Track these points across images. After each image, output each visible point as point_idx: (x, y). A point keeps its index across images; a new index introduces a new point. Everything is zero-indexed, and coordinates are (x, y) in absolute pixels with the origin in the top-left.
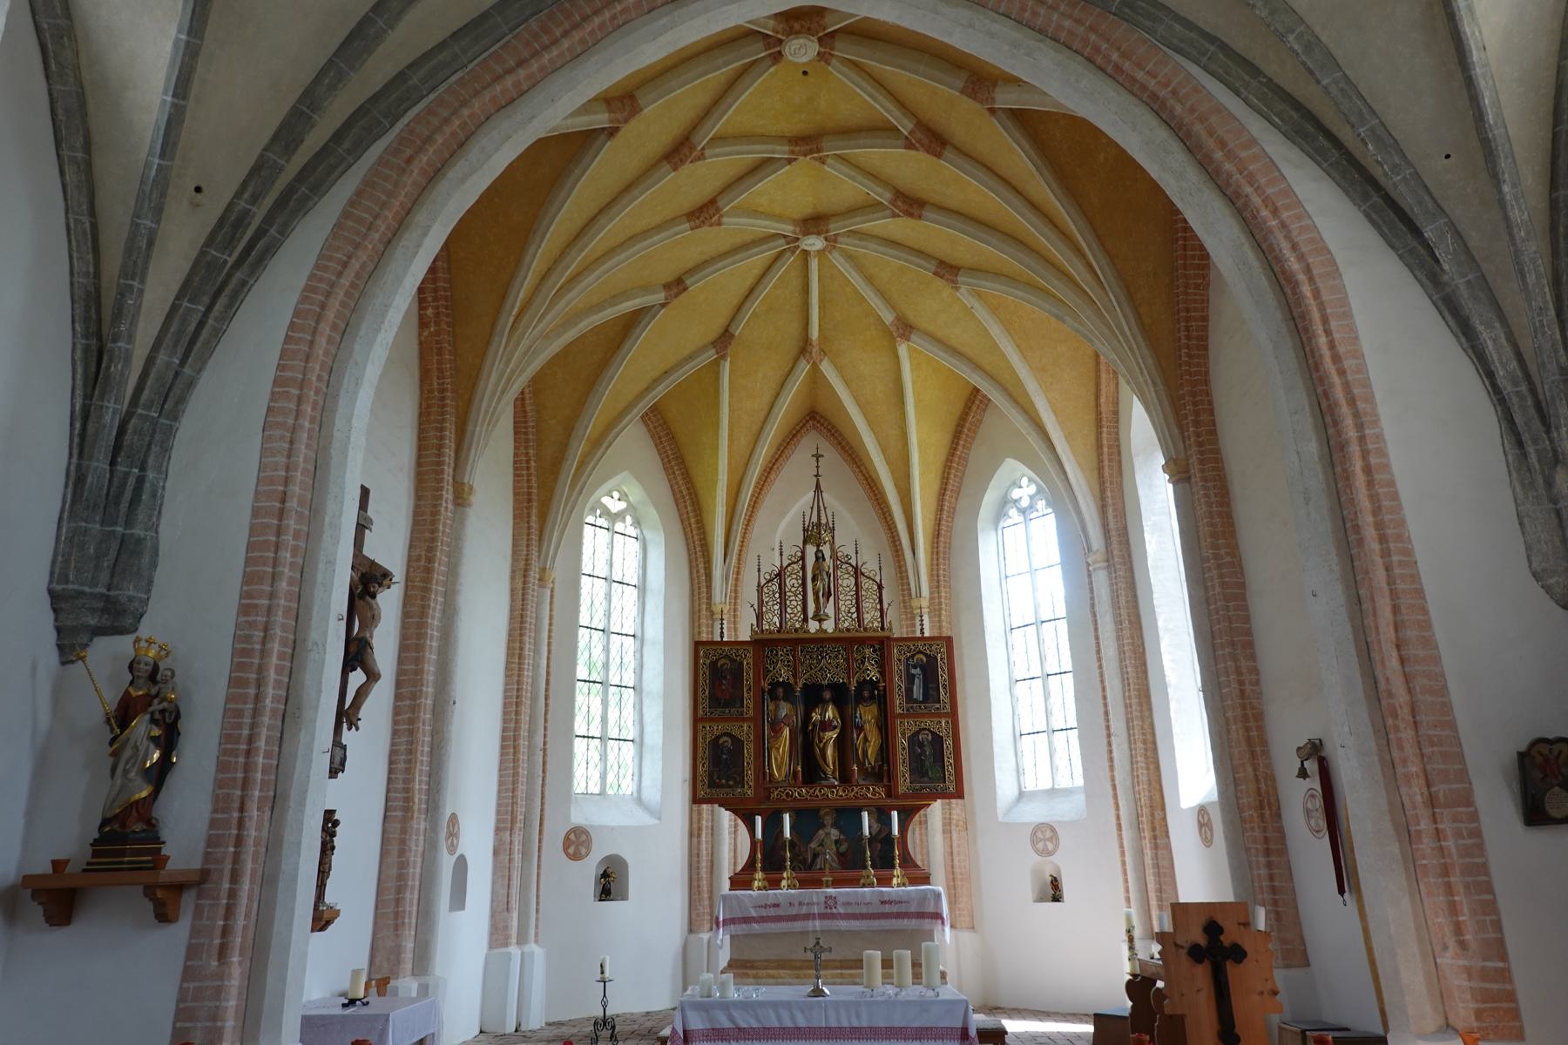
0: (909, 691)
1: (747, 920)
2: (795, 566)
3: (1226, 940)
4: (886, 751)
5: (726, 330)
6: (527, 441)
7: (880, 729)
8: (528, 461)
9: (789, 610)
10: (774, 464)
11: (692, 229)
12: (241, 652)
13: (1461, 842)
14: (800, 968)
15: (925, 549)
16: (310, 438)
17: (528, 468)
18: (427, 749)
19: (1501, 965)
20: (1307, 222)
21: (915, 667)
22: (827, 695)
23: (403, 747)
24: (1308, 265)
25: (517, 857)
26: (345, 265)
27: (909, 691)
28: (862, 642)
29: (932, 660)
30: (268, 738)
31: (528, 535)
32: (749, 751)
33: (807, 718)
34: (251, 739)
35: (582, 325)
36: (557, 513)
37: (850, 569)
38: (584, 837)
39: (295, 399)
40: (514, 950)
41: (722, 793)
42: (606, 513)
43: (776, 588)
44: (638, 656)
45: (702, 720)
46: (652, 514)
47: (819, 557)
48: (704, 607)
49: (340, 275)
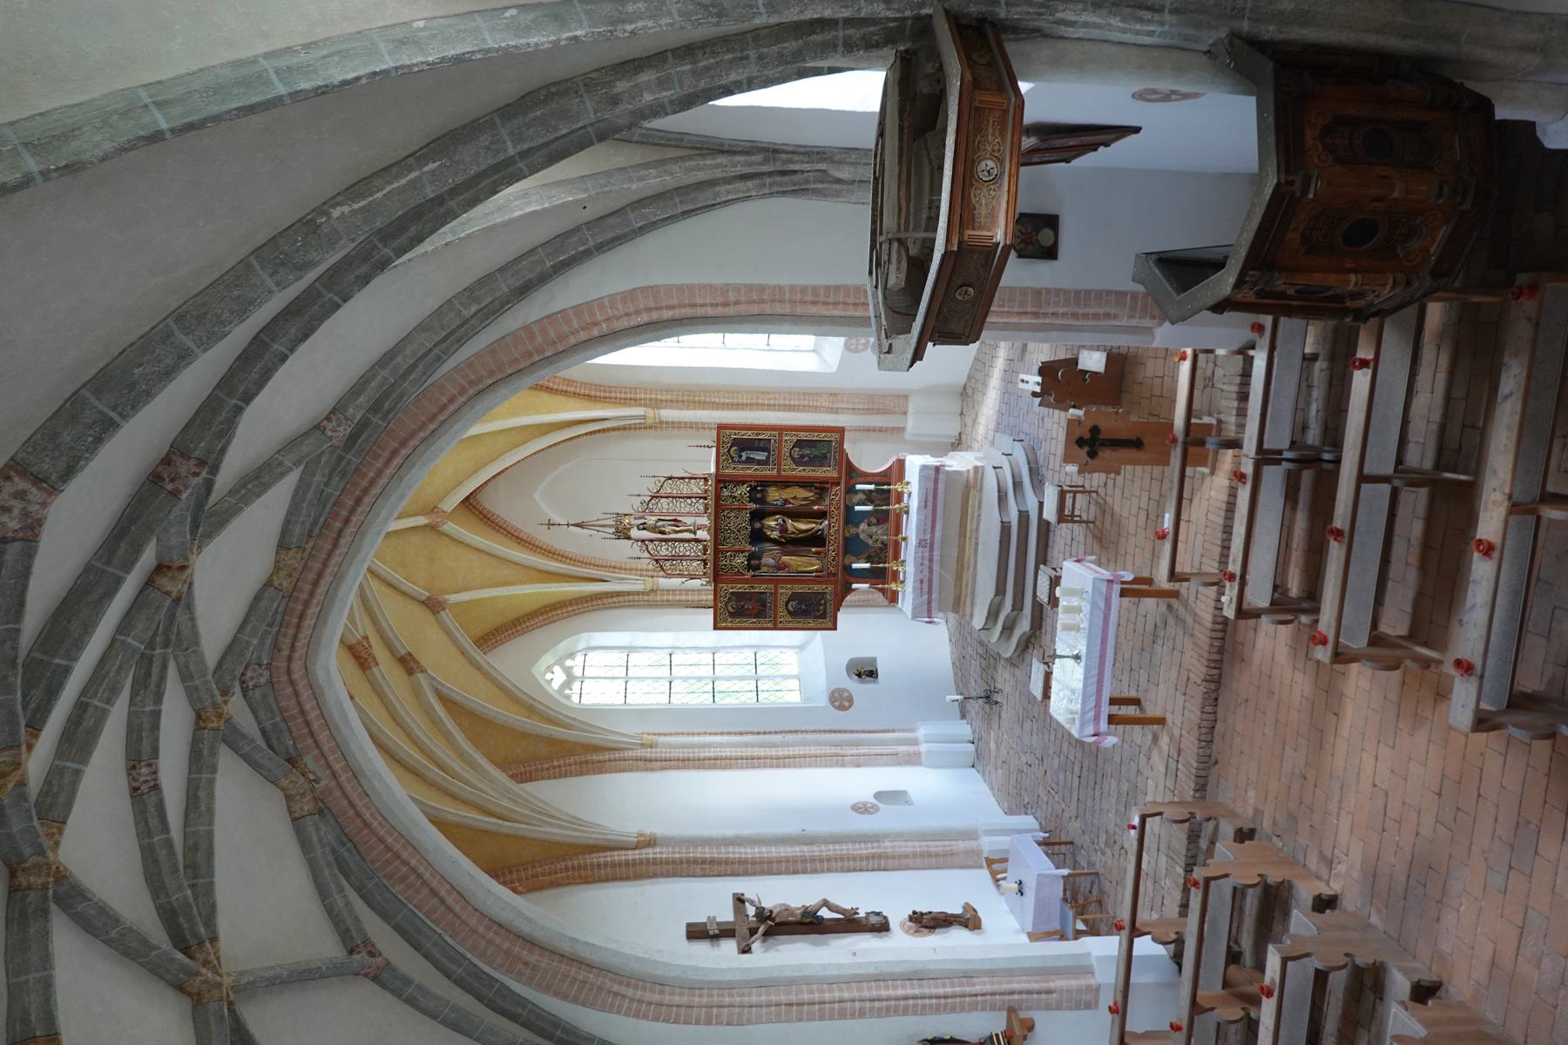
0: (759, 462)
1: (929, 602)
2: (650, 547)
3: (1087, 436)
4: (805, 484)
5: (423, 602)
6: (537, 770)
7: (788, 487)
8: (554, 767)
9: (688, 553)
10: (512, 535)
11: (377, 664)
12: (889, 1012)
13: (1061, 303)
14: (962, 565)
15: (603, 409)
16: (743, 995)
17: (559, 766)
18: (838, 847)
19: (1129, 296)
20: (606, 301)
21: (740, 457)
22: (757, 525)
23: (839, 864)
24: (646, 309)
25: (862, 750)
26: (616, 994)
27: (759, 462)
28: (718, 497)
29: (736, 442)
30: (936, 987)
31: (615, 760)
32: (800, 589)
33: (774, 541)
34: (938, 997)
35: (470, 751)
36: (595, 738)
37: (653, 501)
38: (836, 695)
39: (721, 1010)
40: (923, 748)
41: (830, 609)
42: (568, 684)
43: (668, 564)
44: (687, 651)
45: (775, 624)
46: (564, 646)
47: (643, 527)
48: (646, 598)
49: (624, 996)
